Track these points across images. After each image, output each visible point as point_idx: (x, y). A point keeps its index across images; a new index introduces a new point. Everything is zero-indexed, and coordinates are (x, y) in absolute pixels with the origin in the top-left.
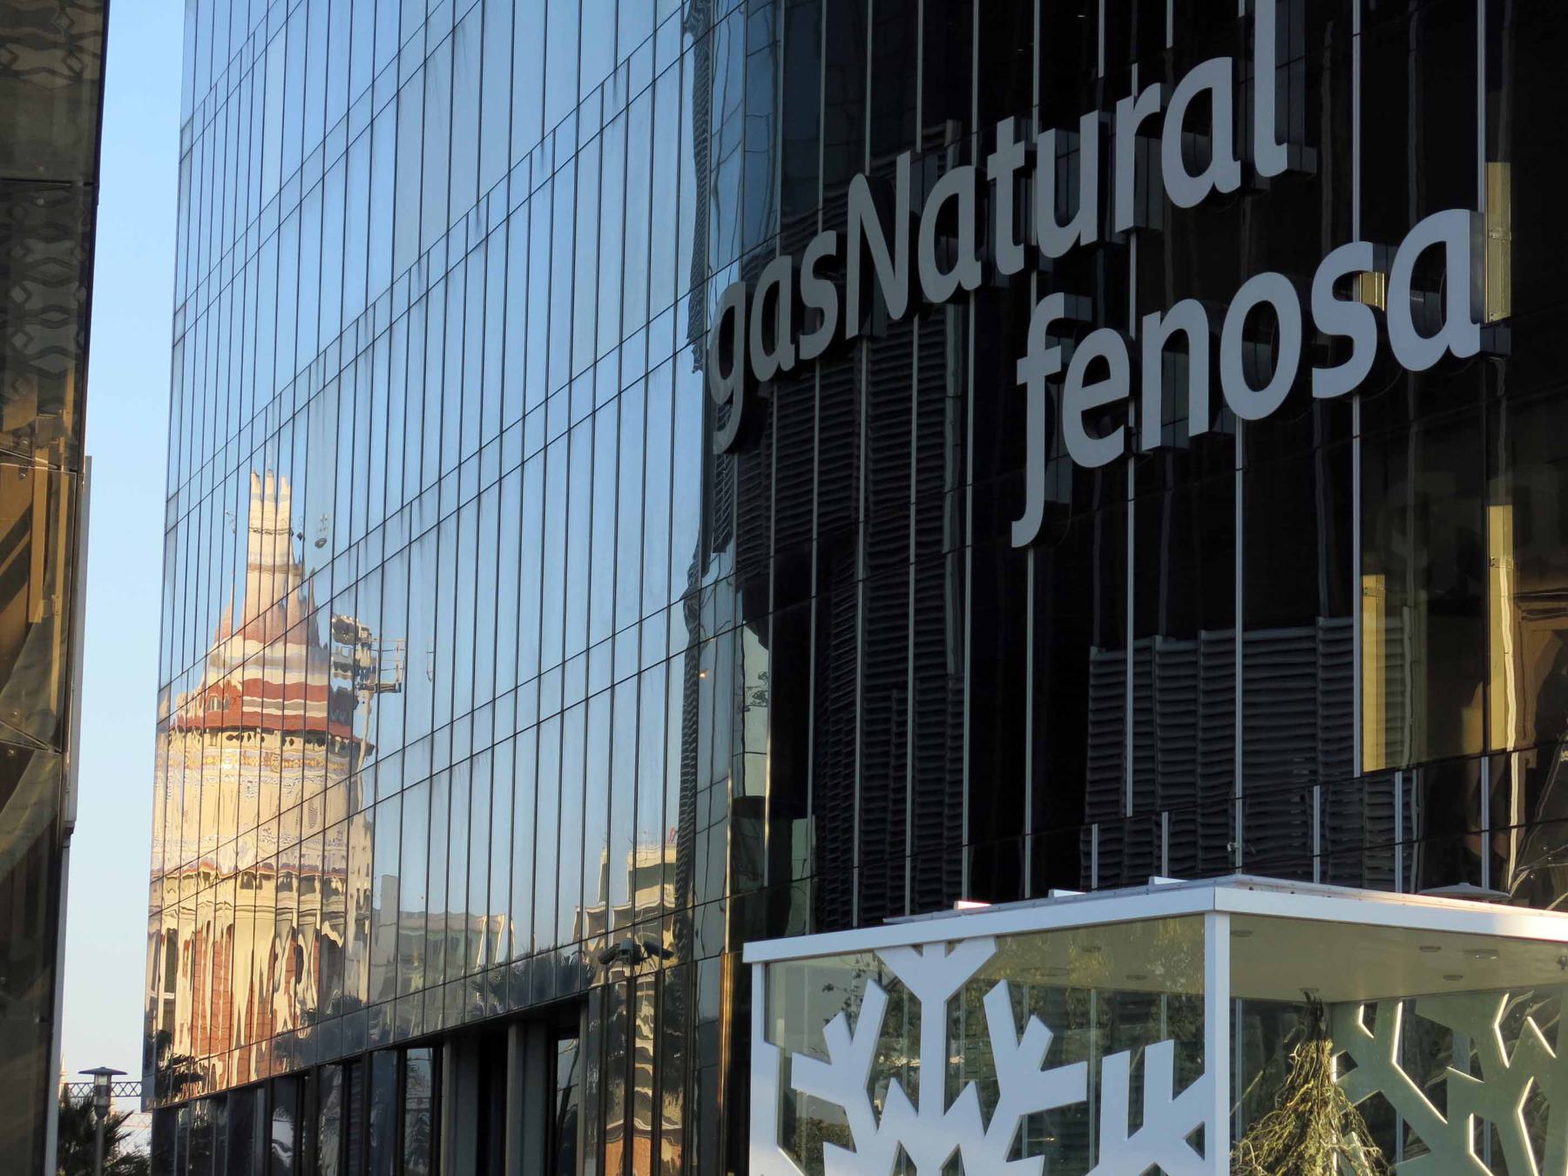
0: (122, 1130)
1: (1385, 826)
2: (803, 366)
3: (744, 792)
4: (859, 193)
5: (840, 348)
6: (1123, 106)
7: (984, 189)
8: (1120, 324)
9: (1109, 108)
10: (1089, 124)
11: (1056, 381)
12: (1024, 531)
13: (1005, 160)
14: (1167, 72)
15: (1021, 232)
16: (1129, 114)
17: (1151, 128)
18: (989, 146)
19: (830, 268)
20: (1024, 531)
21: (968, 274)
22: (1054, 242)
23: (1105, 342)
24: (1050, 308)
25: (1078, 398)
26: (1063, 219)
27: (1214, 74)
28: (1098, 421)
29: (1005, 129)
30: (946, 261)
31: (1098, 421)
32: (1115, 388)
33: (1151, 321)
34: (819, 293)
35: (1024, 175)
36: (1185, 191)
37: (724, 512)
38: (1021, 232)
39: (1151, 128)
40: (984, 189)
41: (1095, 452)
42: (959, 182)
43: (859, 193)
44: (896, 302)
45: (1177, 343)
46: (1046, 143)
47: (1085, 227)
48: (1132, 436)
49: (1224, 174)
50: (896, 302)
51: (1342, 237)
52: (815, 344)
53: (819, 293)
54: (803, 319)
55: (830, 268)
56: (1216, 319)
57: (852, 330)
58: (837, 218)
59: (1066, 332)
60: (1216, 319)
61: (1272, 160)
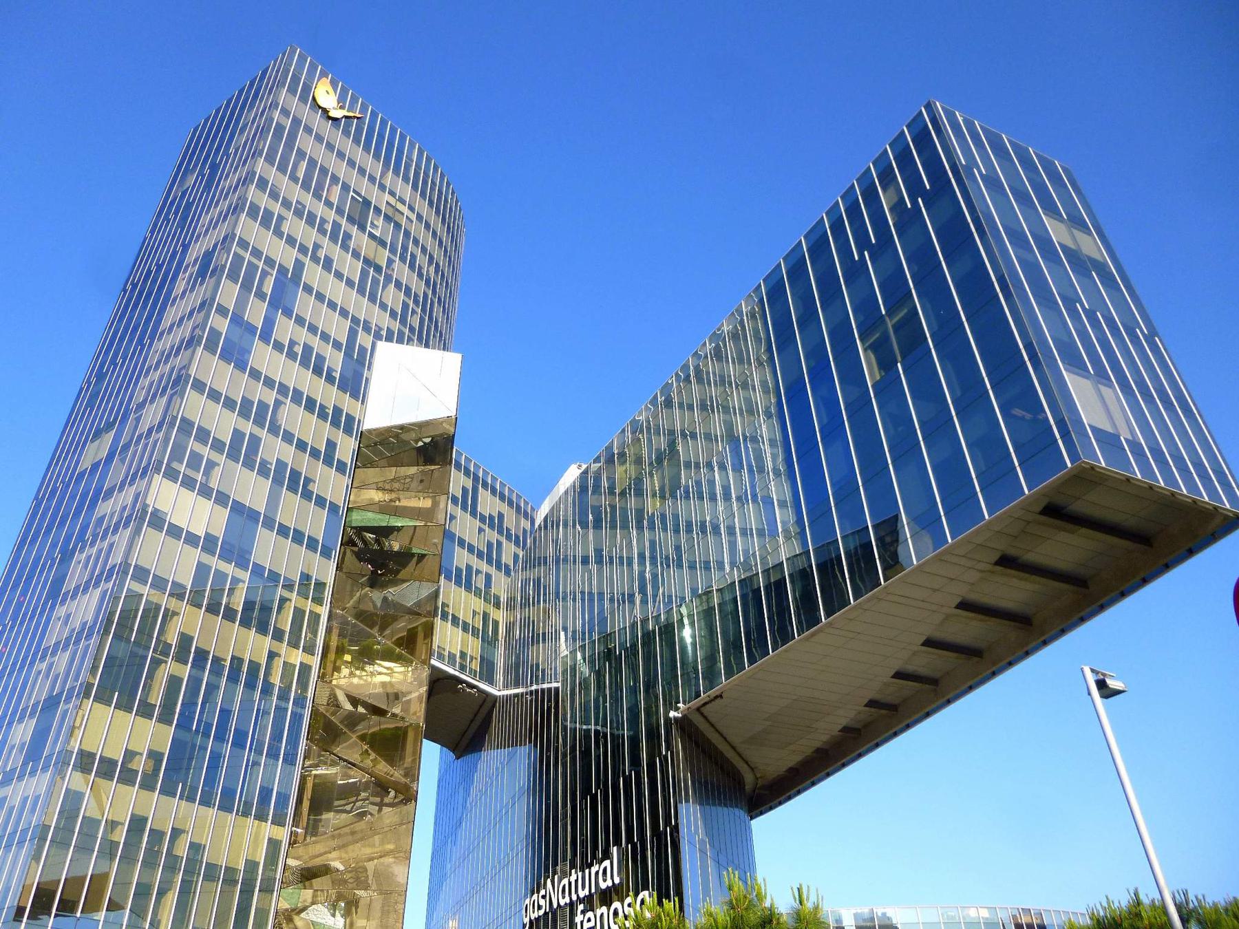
6: (592, 868)
10: (587, 871)
16: (594, 869)
17: (597, 873)
27: (607, 863)
29: (573, 871)
39: (597, 873)
46: (580, 874)
49: (609, 883)
61: (617, 880)
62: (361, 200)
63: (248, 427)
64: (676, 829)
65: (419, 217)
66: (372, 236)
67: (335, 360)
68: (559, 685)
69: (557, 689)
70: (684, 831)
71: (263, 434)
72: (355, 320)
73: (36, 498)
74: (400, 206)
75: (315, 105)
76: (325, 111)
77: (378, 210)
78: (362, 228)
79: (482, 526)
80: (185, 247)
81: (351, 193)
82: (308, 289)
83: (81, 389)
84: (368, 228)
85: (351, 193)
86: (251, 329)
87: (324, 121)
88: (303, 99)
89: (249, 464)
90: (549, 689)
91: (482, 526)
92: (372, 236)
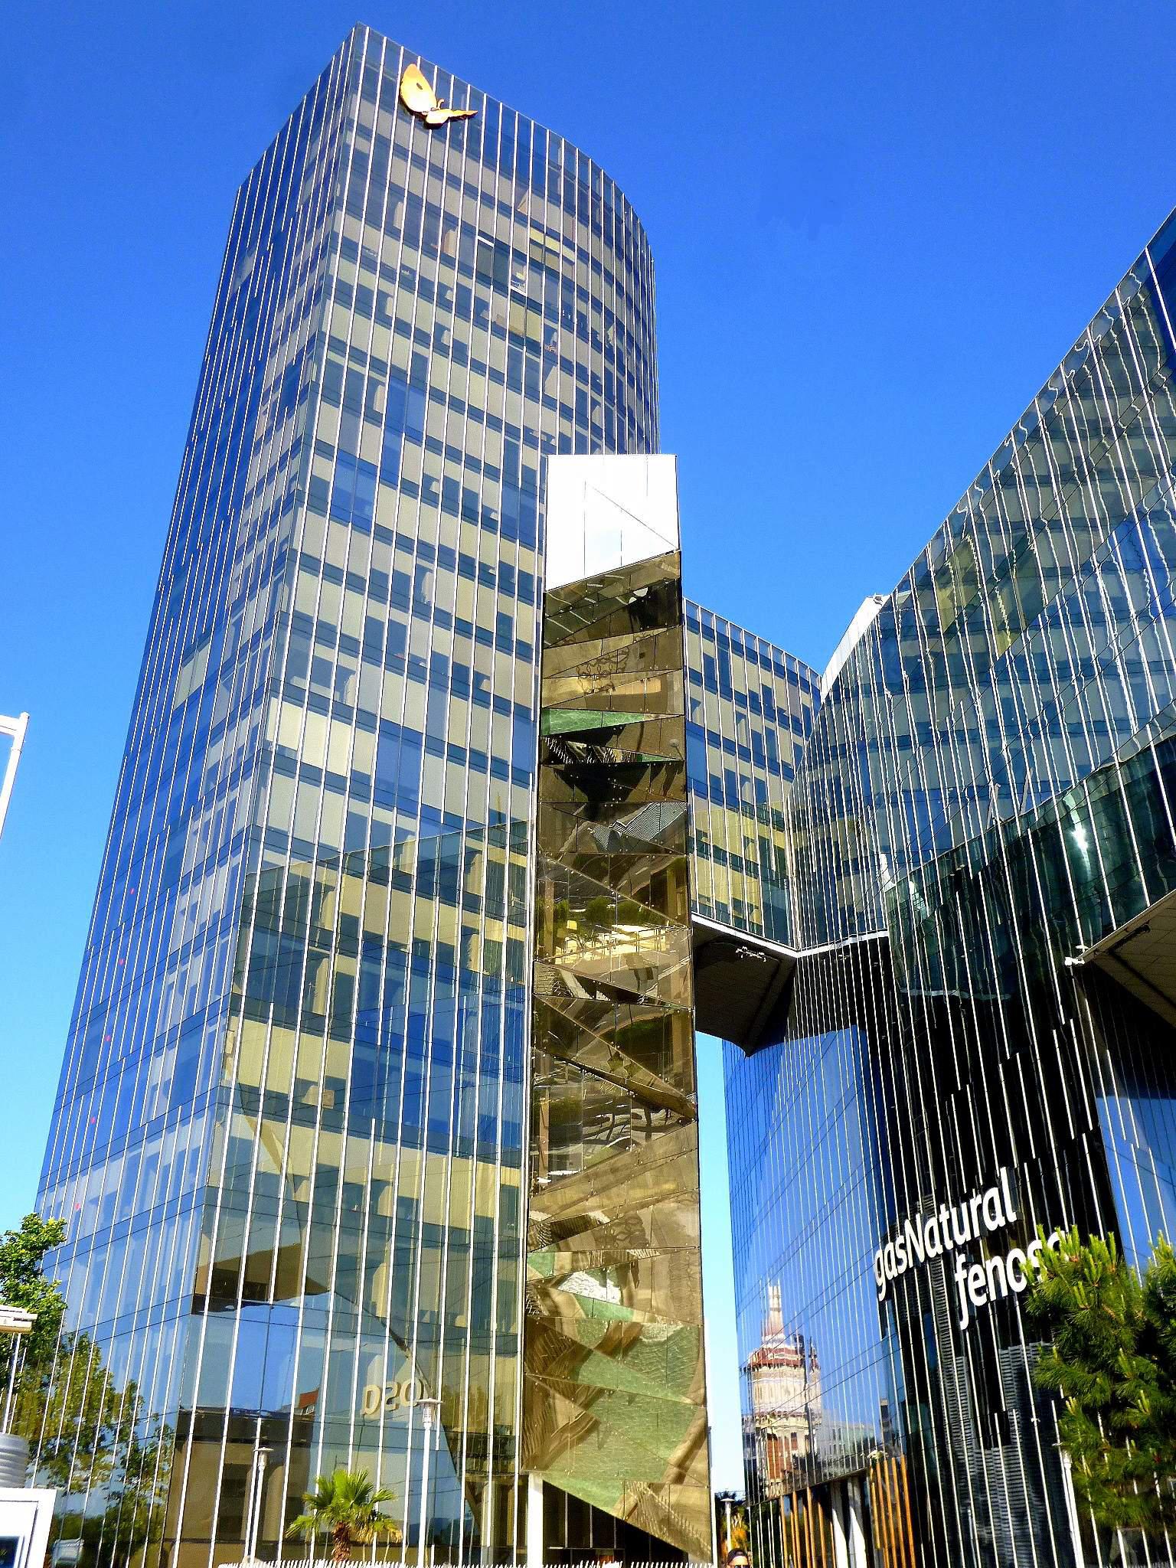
0: (1128, 1409)
1: (979, 1455)
2: (900, 1275)
3: (333, 228)
4: (907, 1224)
5: (909, 1270)
7: (940, 1225)
8: (981, 1264)
9: (968, 1202)
11: (966, 1280)
12: (964, 1324)
13: (944, 1216)
14: (982, 1191)
15: (951, 1236)
16: (975, 1202)
17: (980, 1208)
18: (939, 1212)
19: (903, 1246)
20: (964, 1324)
21: (939, 1249)
22: (960, 1240)
23: (976, 1269)
24: (961, 1259)
25: (973, 1286)
26: (961, 1233)
27: (993, 1192)
28: (979, 1292)
30: (933, 1245)
31: (979, 1292)
32: (981, 1283)
33: (988, 1262)
34: (901, 1254)
35: (950, 1221)
36: (992, 1226)
37: (620, 384)
38: (951, 1236)
39: (980, 1208)
40: (940, 1225)
41: (979, 1301)
42: (932, 1222)
43: (907, 1224)
44: (922, 1258)
45: (995, 1268)
46: (954, 1211)
47: (967, 1236)
48: (988, 1296)
50: (922, 1258)
51: (1032, 1238)
52: (902, 1269)
53: (901, 1254)
54: (899, 1262)
55: (903, 1246)
56: (1005, 1261)
57: (911, 1265)
58: (903, 1233)
59: (965, 1266)
60: (1005, 1261)
61: (1012, 1217)
62: (492, 245)
63: (384, 613)
64: (1096, 1137)
65: (583, 255)
66: (517, 298)
67: (492, 495)
68: (887, 934)
69: (884, 940)
70: (1110, 1141)
71: (406, 618)
72: (512, 431)
73: (127, 752)
74: (551, 244)
75: (406, 110)
76: (421, 117)
77: (520, 256)
78: (501, 288)
79: (742, 710)
80: (260, 366)
81: (478, 237)
82: (438, 396)
83: (158, 594)
84: (510, 287)
85: (478, 237)
86: (367, 469)
87: (421, 134)
88: (386, 106)
89: (395, 666)
90: (873, 942)
91: (742, 710)
92: (517, 298)
